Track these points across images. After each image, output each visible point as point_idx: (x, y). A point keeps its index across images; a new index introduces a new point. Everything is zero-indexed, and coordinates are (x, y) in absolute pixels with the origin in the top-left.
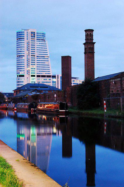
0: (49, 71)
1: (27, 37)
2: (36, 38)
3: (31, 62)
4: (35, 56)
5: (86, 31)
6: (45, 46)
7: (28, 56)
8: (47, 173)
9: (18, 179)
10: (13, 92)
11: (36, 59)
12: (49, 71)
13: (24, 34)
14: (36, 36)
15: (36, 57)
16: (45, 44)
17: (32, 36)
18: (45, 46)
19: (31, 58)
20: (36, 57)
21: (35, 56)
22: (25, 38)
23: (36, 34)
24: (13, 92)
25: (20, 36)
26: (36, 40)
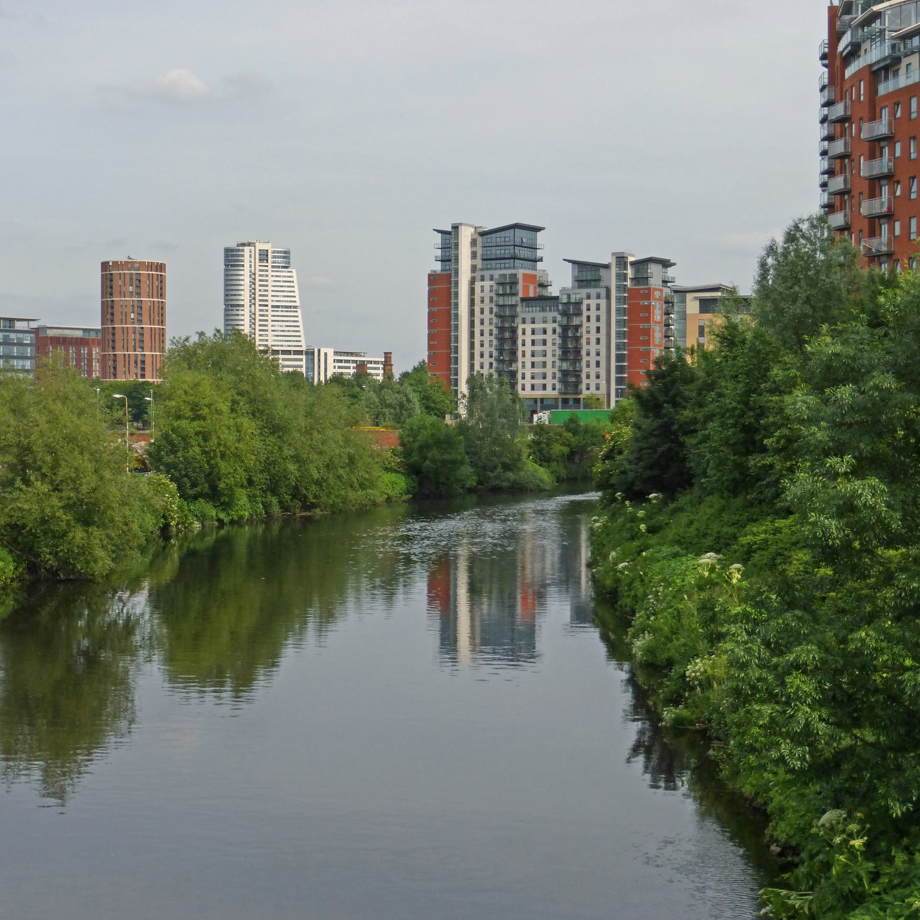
0: (299, 341)
1: (250, 256)
2: (270, 264)
3: (260, 320)
4: (267, 306)
5: (385, 353)
6: (290, 282)
7: (253, 306)
8: (843, 29)
9: (824, 153)
10: (684, 782)
11: (270, 313)
12: (299, 341)
13: (243, 256)
14: (270, 259)
15: (269, 308)
16: (290, 277)
17: (261, 260)
18: (290, 282)
19: (261, 310)
20: (269, 308)
21: (267, 306)
22: (247, 264)
23: (270, 255)
24: (684, 782)
25: (232, 258)
26: (269, 268)
